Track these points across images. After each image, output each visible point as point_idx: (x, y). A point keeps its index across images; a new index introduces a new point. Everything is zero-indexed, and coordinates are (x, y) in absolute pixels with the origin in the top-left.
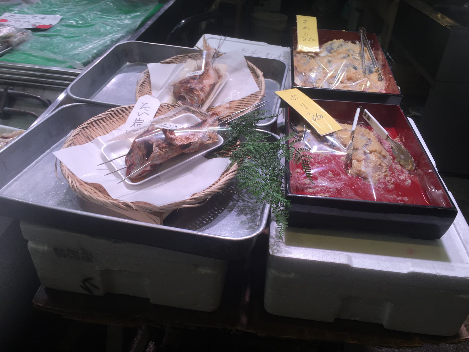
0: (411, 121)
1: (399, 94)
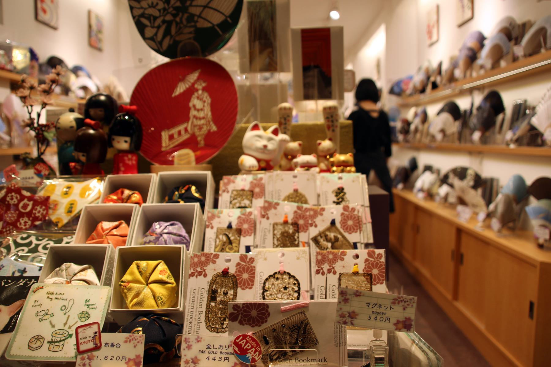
0: (239, 353)
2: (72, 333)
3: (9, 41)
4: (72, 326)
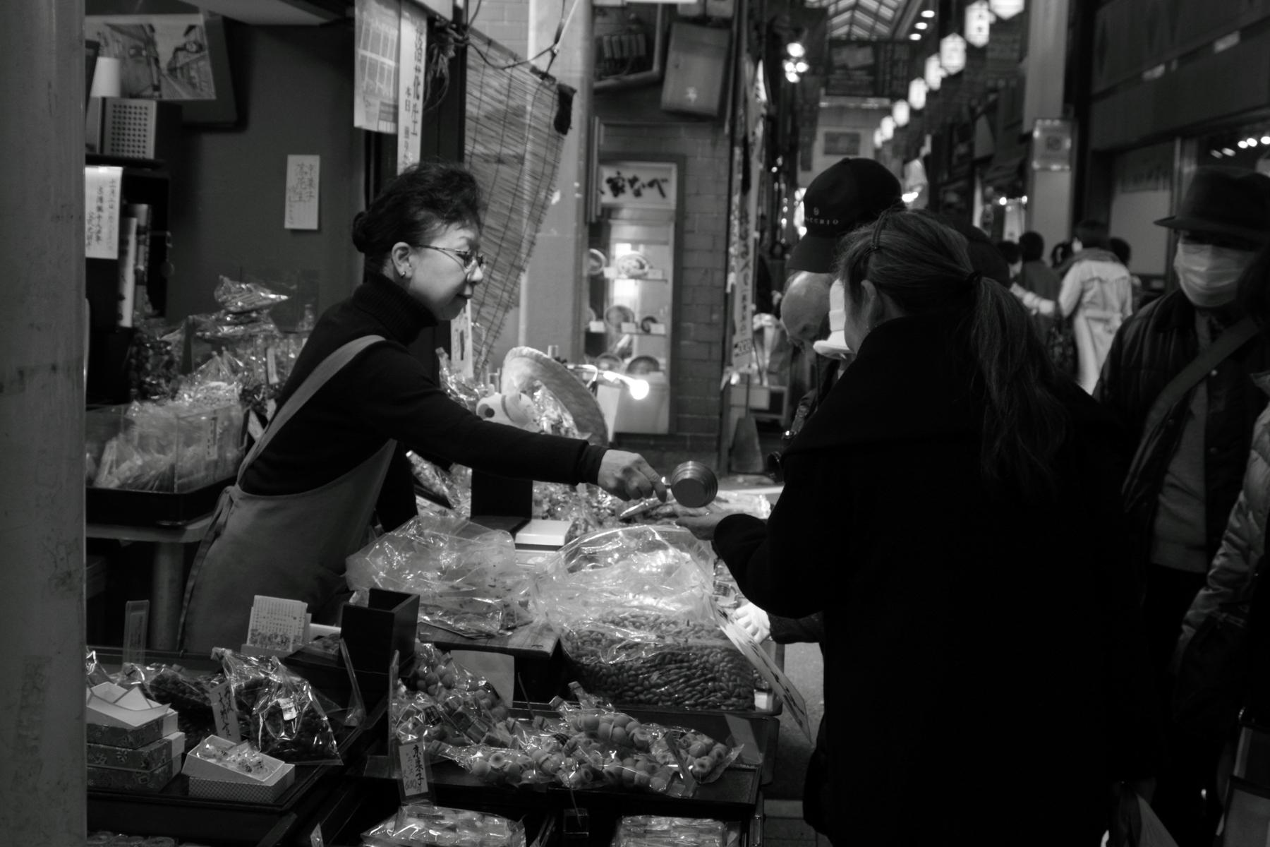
1: (190, 793)
2: (92, 413)
3: (535, 490)
4: (121, 707)
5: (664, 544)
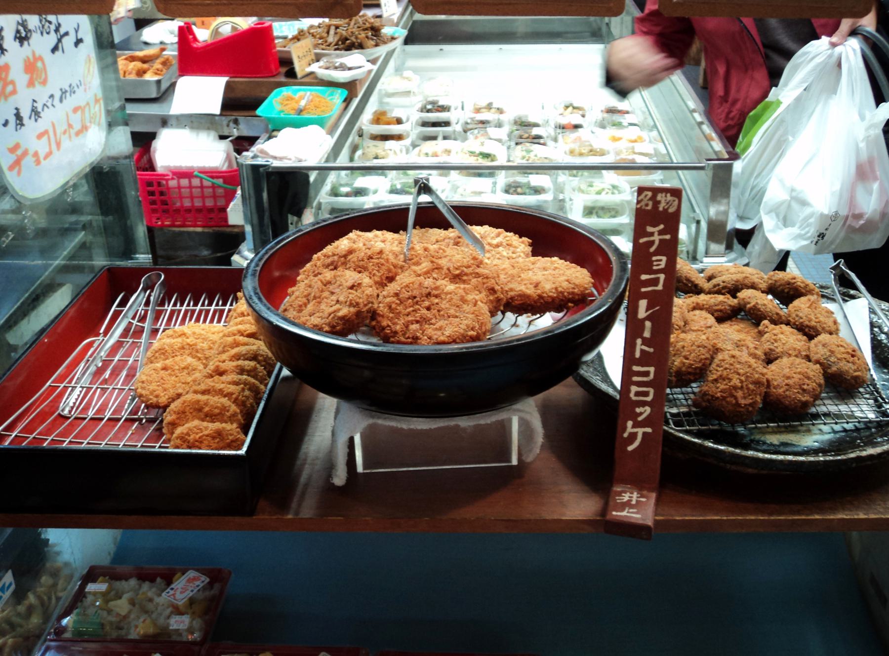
0: (651, 350)
5: (342, 334)
